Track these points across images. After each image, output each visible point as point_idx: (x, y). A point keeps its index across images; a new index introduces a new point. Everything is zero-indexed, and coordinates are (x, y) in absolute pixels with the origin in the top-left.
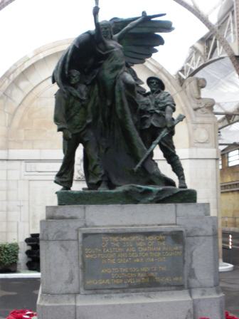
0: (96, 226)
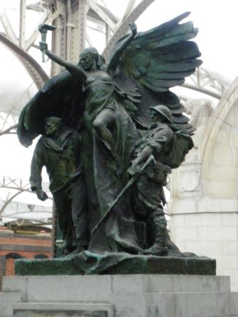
0: (35, 301)
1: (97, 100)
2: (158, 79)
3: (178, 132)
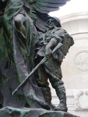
1: (14, 7)
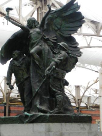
1: (33, 42)
2: (66, 31)
3: (70, 55)
